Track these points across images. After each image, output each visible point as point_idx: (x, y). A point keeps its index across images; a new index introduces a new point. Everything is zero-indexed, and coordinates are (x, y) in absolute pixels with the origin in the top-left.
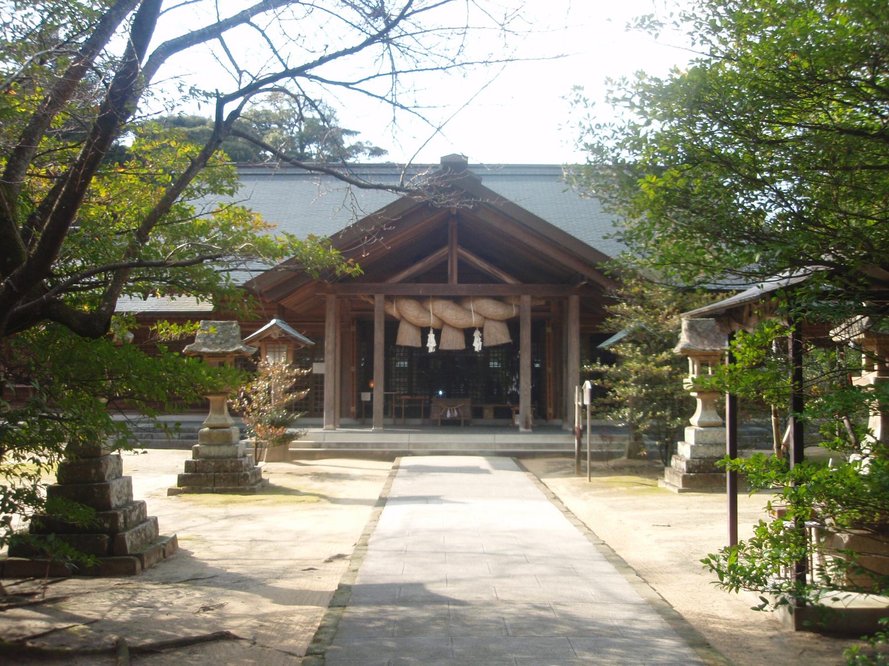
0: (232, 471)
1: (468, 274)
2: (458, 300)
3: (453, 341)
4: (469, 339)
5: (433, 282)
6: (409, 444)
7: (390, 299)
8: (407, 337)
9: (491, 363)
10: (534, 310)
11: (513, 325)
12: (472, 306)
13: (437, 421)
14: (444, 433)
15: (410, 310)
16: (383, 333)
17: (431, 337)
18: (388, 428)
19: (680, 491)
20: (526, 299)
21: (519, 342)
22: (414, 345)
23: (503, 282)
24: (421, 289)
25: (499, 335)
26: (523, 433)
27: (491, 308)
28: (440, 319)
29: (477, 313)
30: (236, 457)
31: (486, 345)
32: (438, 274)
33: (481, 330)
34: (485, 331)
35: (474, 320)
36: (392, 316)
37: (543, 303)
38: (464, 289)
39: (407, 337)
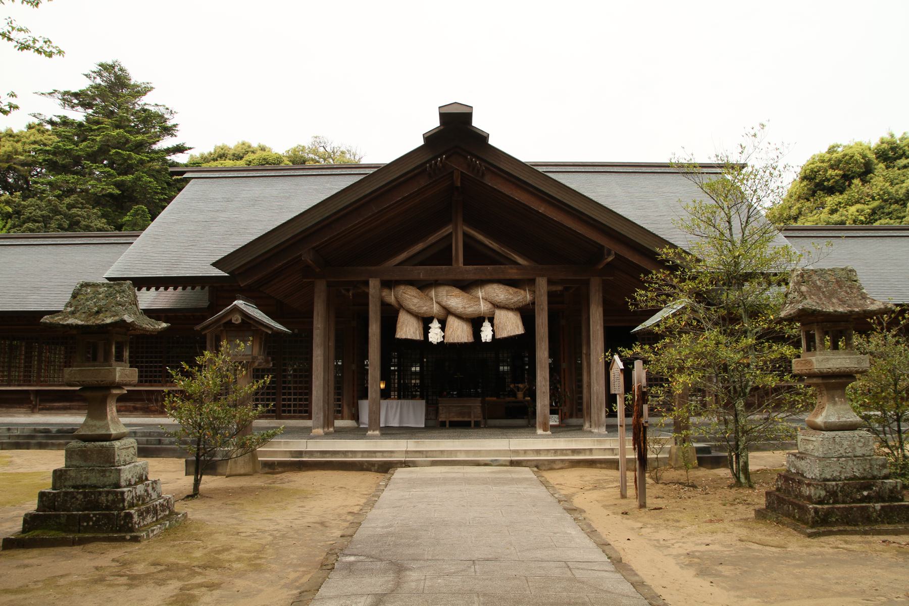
0: (108, 508)
1: (474, 254)
2: (466, 286)
3: (459, 332)
4: (477, 332)
5: (436, 267)
6: (407, 452)
7: (388, 284)
8: (408, 329)
9: (501, 368)
10: (551, 295)
11: (527, 314)
12: (480, 293)
13: (445, 422)
14: (449, 438)
15: (411, 298)
16: (379, 324)
17: (435, 326)
18: (556, 430)
19: (761, 515)
20: (542, 284)
21: (492, 431)
22: (414, 338)
23: (515, 263)
24: (421, 272)
25: (510, 325)
26: (542, 436)
27: (500, 293)
28: (444, 308)
29: (485, 299)
30: (118, 486)
31: (498, 336)
32: (442, 256)
33: (491, 320)
34: (496, 321)
35: (484, 307)
36: (389, 305)
37: (560, 288)
38: (472, 272)
39: (408, 329)
